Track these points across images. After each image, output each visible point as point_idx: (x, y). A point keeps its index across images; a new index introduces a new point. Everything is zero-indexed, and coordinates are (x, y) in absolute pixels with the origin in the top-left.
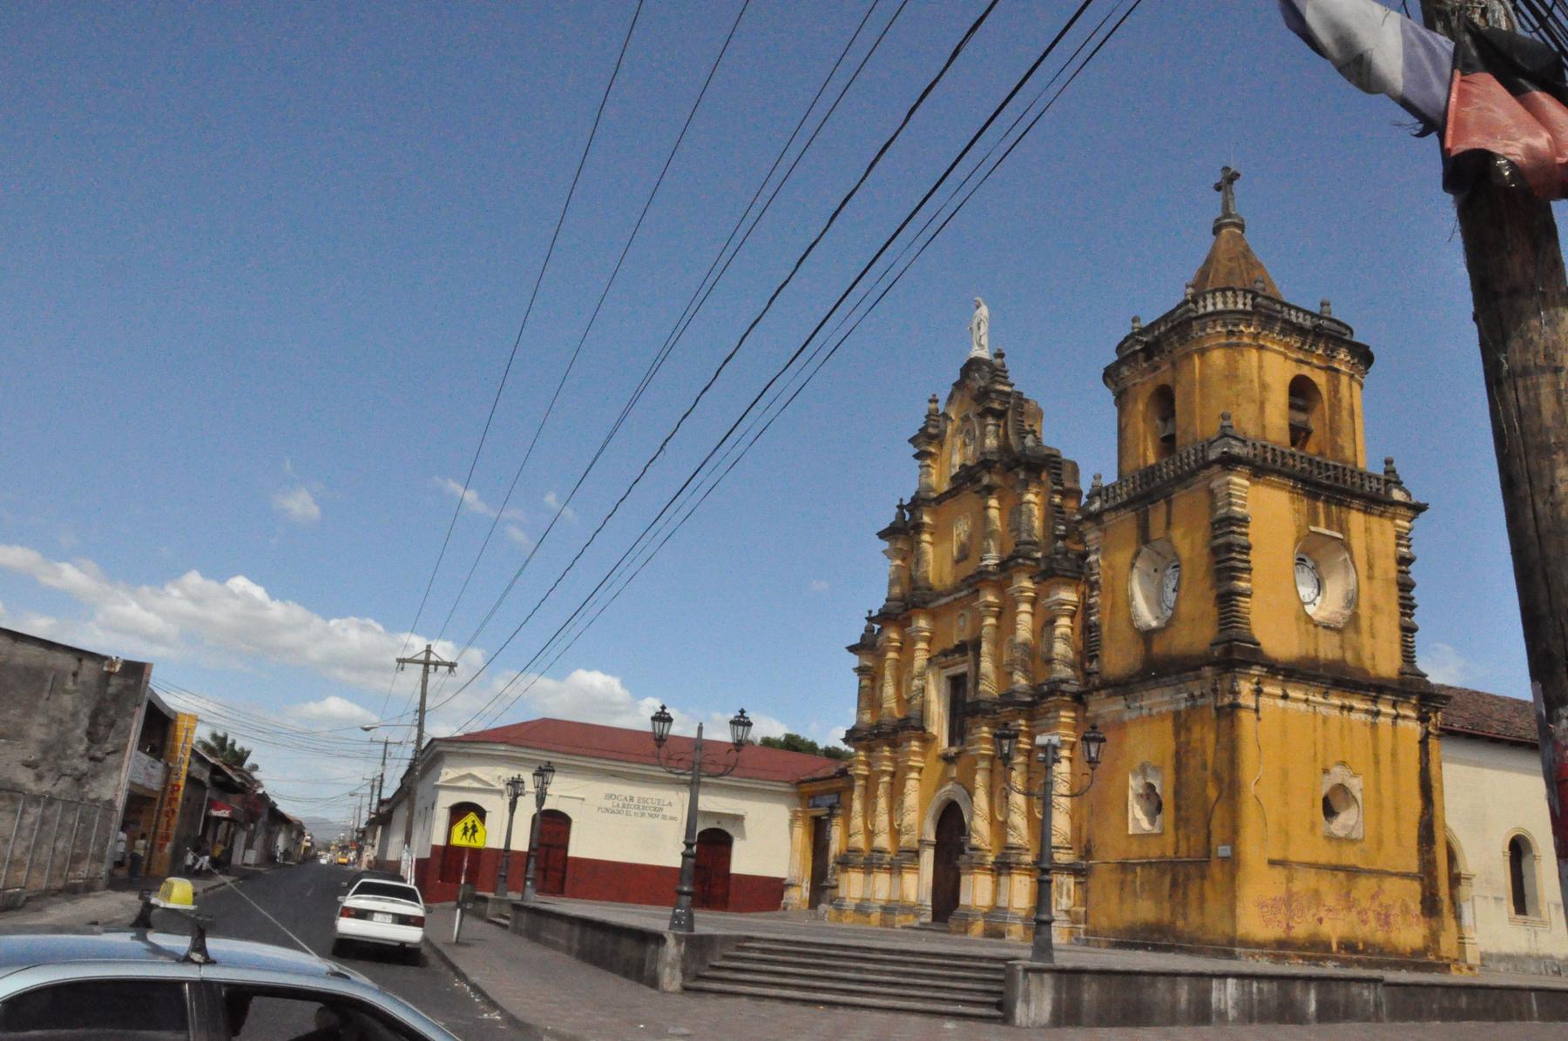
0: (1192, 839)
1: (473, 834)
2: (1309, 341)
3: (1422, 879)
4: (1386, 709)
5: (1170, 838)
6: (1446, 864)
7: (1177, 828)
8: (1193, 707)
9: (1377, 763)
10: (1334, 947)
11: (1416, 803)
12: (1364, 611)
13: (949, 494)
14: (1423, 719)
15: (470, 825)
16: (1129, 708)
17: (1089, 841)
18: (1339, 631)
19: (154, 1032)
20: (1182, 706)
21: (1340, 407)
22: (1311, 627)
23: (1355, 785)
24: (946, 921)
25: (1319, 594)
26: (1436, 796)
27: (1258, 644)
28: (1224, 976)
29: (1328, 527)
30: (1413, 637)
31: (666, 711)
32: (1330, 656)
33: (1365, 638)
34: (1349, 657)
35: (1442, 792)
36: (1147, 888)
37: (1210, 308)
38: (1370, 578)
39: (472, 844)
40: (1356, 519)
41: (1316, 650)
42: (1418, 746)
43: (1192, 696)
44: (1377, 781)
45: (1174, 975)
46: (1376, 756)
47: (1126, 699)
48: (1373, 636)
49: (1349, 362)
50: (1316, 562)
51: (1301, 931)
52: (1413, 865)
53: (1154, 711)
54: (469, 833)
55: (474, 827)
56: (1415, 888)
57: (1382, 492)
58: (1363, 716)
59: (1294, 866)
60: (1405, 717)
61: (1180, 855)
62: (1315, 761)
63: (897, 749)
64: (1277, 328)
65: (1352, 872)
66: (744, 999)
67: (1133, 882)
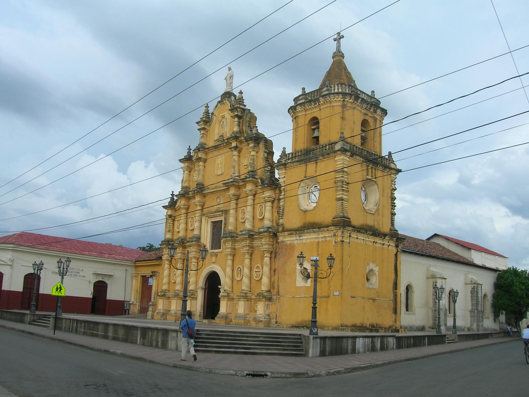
1: (60, 290)
4: (386, 243)
6: (317, 288)
13: (216, 147)
14: (397, 246)
15: (59, 287)
23: (376, 269)
24: (214, 319)
28: (360, 337)
37: (336, 91)
39: (60, 294)
40: (379, 173)
42: (394, 256)
45: (348, 337)
50: (365, 188)
54: (59, 290)
55: (60, 287)
57: (388, 164)
58: (379, 245)
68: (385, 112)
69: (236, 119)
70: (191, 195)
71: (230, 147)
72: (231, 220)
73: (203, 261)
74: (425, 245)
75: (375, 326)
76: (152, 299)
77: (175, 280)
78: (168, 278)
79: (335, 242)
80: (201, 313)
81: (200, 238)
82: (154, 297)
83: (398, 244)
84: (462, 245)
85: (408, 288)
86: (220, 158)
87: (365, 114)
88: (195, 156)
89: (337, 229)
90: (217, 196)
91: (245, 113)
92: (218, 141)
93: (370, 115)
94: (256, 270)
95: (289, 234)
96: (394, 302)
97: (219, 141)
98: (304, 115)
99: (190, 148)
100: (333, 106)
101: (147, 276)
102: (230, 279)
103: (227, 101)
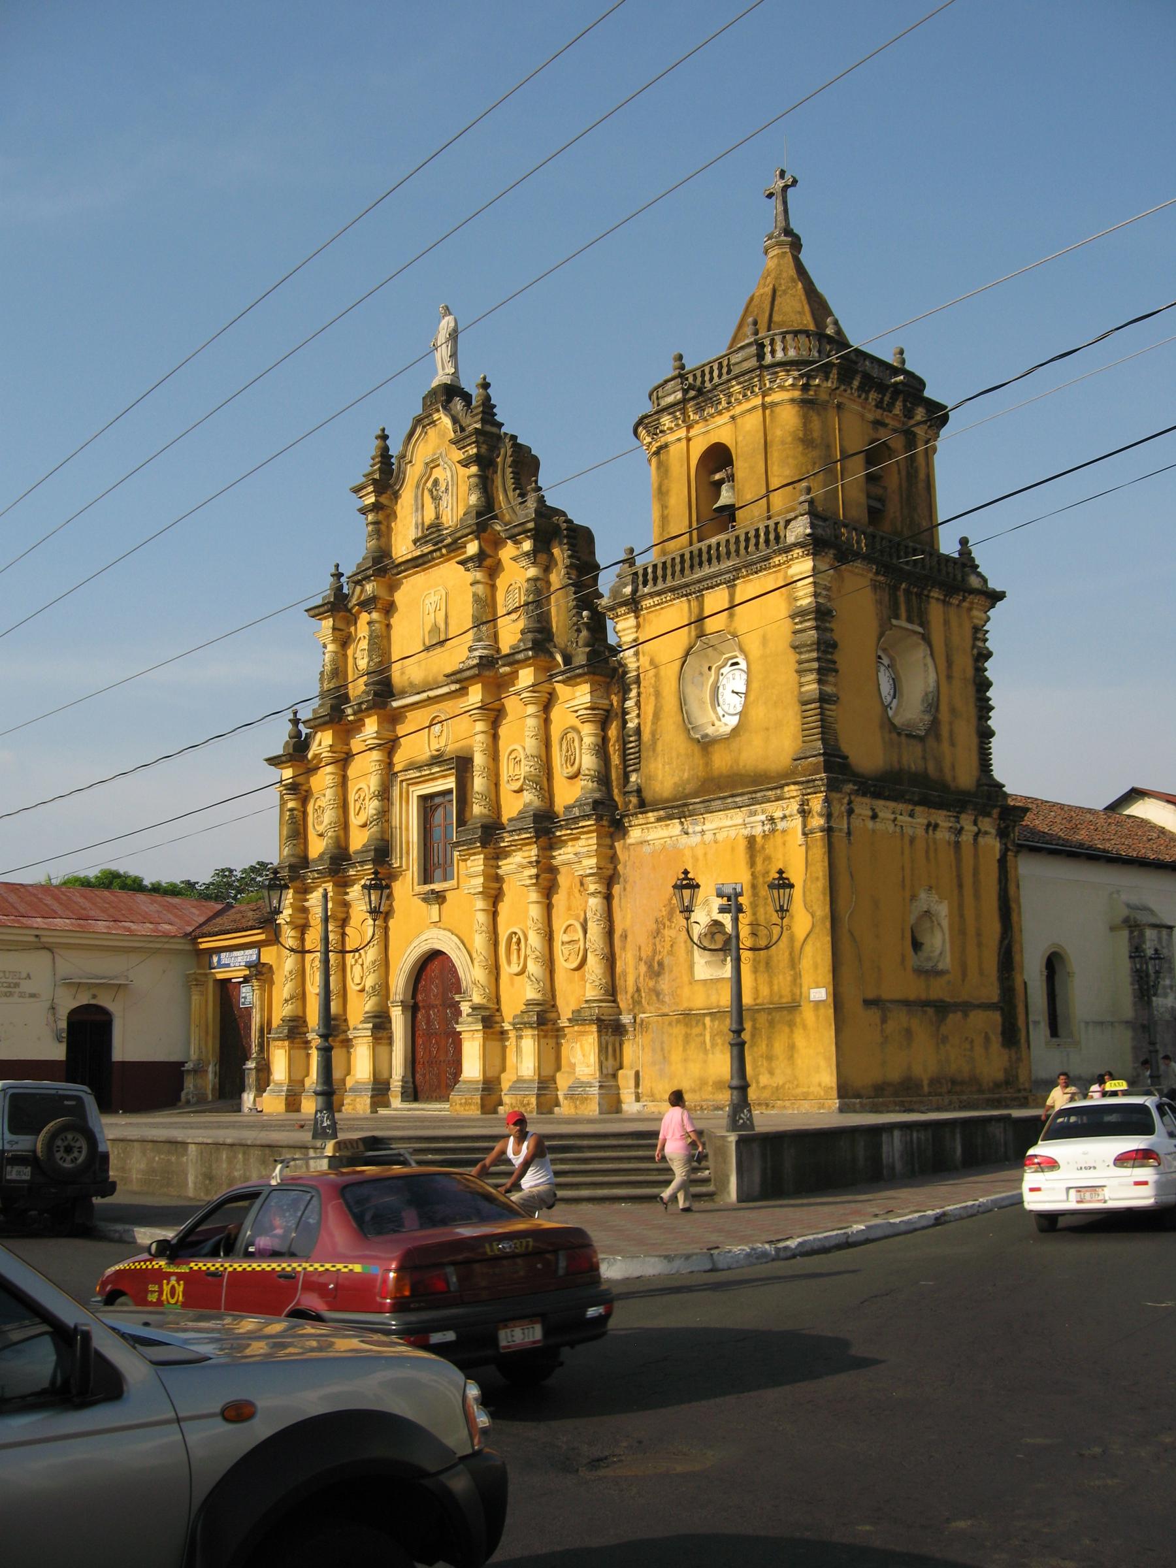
3: (1002, 1009)
8: (773, 831)
9: (960, 886)
11: (993, 927)
12: (944, 715)
16: (687, 833)
18: (921, 739)
20: (758, 831)
21: (916, 477)
22: (894, 735)
25: (894, 697)
26: (1014, 917)
27: (845, 758)
29: (910, 620)
30: (990, 742)
33: (945, 746)
35: (1019, 913)
36: (719, 1041)
38: (949, 677)
43: (772, 820)
44: (961, 906)
46: (959, 877)
47: (682, 823)
48: (953, 744)
50: (892, 659)
52: (992, 993)
53: (720, 837)
56: (997, 1017)
59: (888, 1005)
60: (986, 833)
62: (903, 887)
64: (856, 383)
65: (941, 1009)
67: (702, 1035)
68: (938, 416)
69: (474, 469)
76: (254, 1049)
79: (805, 834)
85: (1053, 964)
87: (878, 424)
94: (566, 938)
95: (659, 820)
100: (774, 405)
101: (233, 980)
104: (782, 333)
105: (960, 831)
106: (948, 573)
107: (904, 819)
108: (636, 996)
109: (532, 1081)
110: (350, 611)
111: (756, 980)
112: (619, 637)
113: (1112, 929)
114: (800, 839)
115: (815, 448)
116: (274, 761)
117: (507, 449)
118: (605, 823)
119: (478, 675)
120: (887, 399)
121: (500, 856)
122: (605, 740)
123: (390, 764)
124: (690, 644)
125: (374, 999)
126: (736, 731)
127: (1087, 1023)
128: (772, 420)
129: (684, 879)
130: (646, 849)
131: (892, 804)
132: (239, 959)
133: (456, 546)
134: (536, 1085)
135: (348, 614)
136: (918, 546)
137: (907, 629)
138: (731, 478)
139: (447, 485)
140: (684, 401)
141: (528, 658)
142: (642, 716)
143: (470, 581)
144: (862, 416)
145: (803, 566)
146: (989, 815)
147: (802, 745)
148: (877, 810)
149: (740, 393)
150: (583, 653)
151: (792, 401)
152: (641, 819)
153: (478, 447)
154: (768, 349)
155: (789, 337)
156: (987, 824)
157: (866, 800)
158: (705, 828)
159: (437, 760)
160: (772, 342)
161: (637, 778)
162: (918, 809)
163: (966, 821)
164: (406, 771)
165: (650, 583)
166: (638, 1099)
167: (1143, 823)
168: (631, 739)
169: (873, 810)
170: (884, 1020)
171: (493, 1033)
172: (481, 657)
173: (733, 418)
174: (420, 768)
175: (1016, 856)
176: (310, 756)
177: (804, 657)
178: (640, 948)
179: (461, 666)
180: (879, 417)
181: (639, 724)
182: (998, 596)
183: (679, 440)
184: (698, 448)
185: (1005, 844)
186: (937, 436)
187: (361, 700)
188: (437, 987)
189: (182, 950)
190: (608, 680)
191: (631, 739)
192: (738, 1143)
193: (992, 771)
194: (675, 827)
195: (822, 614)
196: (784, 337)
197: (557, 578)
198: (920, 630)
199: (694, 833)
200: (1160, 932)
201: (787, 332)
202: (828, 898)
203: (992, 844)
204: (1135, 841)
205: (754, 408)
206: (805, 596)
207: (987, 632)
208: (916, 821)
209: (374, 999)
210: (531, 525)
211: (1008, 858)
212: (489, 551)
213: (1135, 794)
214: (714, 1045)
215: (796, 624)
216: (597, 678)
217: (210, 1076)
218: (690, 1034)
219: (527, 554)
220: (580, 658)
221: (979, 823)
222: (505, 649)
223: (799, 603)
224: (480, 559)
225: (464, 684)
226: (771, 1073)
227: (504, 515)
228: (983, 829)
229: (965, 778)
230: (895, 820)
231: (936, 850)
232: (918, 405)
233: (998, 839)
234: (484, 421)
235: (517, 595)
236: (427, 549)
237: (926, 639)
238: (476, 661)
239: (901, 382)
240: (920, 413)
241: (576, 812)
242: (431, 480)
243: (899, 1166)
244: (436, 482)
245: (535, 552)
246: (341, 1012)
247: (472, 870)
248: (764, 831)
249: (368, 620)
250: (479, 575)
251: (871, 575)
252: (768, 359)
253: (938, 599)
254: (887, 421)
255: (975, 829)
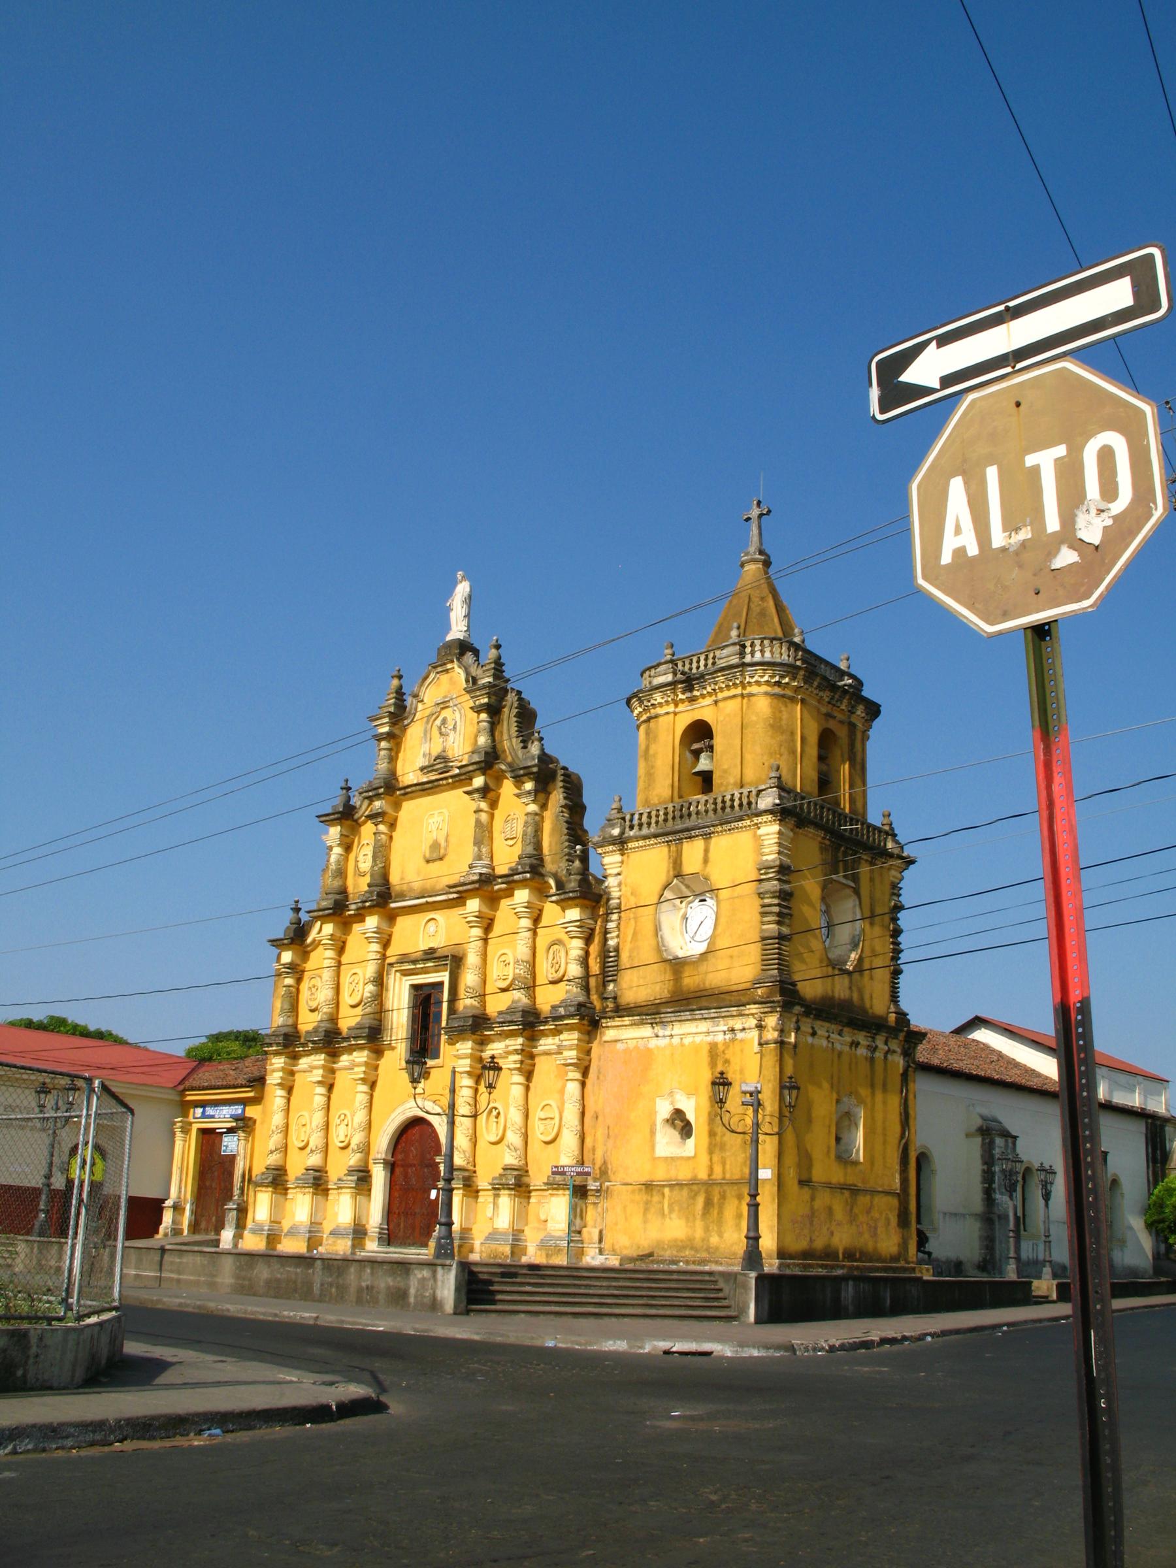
0: (728, 1162)
2: (837, 696)
5: (704, 1158)
7: (711, 1152)
8: (733, 1040)
10: (841, 1256)
11: (897, 1128)
17: (605, 1163)
19: (459, 1336)
20: (720, 1038)
30: (899, 978)
31: (495, 1060)
32: (842, 996)
34: (855, 996)
36: (676, 1208)
41: (833, 992)
43: (733, 1030)
49: (863, 718)
51: (819, 1244)
56: (895, 1202)
60: (894, 1052)
61: (714, 1177)
63: (336, 1059)
66: (523, 1315)
67: (661, 1203)
68: (873, 710)
69: (484, 716)
70: (352, 912)
71: (469, 789)
72: (469, 978)
73: (490, 1093)
74: (954, 1048)
75: (858, 1255)
76: (236, 1192)
77: (303, 1141)
78: (322, 1134)
79: (760, 1044)
80: (382, 1229)
81: (380, 1029)
82: (242, 1189)
83: (909, 1049)
84: (1033, 1041)
86: (436, 815)
87: (829, 716)
88: (364, 807)
89: (766, 1010)
90: (425, 921)
91: (506, 701)
92: (457, 779)
93: (839, 716)
96: (902, 1197)
97: (434, 770)
98: (672, 715)
99: (349, 785)
100: (751, 695)
101: (218, 1131)
102: (468, 1138)
103: (455, 665)
104: (760, 639)
105: (874, 1049)
106: (828, 820)
107: (834, 1036)
108: (603, 1168)
109: (504, 1234)
110: (356, 821)
111: (711, 1160)
112: (605, 869)
113: (968, 1136)
114: (756, 1048)
115: (782, 733)
116: (277, 943)
117: (511, 698)
118: (585, 1022)
119: (477, 889)
120: (837, 696)
121: (485, 1042)
122: (587, 953)
123: (384, 957)
124: (668, 881)
125: (358, 1155)
126: (704, 956)
127: (945, 1214)
128: (748, 707)
129: (720, 1078)
130: (619, 1046)
131: (826, 1024)
132: (224, 1112)
133: (463, 778)
134: (511, 1237)
135: (354, 823)
136: (854, 817)
137: (843, 884)
138: (711, 748)
139: (455, 724)
140: (673, 684)
141: (525, 880)
142: (621, 936)
143: (475, 809)
144: (818, 710)
145: (770, 830)
146: (896, 1037)
147: (761, 972)
148: (816, 1029)
149: (723, 682)
150: (575, 880)
151: (766, 694)
152: (617, 1022)
153: (489, 698)
154: (748, 650)
155: (766, 642)
156: (895, 1045)
157: (808, 1020)
158: (673, 1033)
159: (430, 954)
160: (752, 645)
161: (614, 987)
162: (846, 1029)
163: (880, 1041)
164: (402, 963)
165: (636, 828)
166: (601, 1252)
167: (986, 1047)
168: (611, 954)
169: (813, 1028)
170: (813, 1199)
171: (470, 1191)
172: (481, 874)
173: (716, 702)
174: (414, 962)
175: (914, 1072)
176: (309, 940)
177: (767, 901)
178: (608, 1128)
179: (462, 880)
180: (830, 711)
181: (619, 943)
182: (910, 862)
183: (668, 713)
184: (684, 720)
185: (908, 1062)
186: (871, 727)
187: (364, 899)
188: (416, 1149)
189: (173, 1100)
190: (594, 904)
191: (611, 954)
192: (757, 1279)
193: (899, 1001)
194: (646, 1031)
195: (784, 871)
196: (762, 642)
197: (549, 817)
198: (852, 884)
199: (664, 1036)
200: (1006, 1141)
201: (765, 638)
202: (778, 1098)
203: (899, 1061)
204: (981, 1063)
205: (735, 696)
206: (771, 855)
207: (901, 888)
208: (842, 1040)
209: (358, 1155)
210: (535, 769)
211: (909, 1073)
212: (492, 785)
213: (978, 1022)
214: (671, 1211)
215: (761, 874)
216: (586, 902)
217: (187, 1213)
218: (651, 1201)
219: (529, 793)
220: (572, 884)
221: (889, 1044)
222: (501, 870)
223: (765, 858)
224: (485, 791)
225: (463, 895)
226: (721, 1235)
227: (507, 757)
228: (892, 1048)
229: (879, 1005)
230: (829, 1037)
231: (856, 1063)
232: (859, 704)
233: (902, 1057)
234: (496, 677)
235: (515, 825)
236: (433, 776)
237: (857, 892)
238: (476, 878)
239: (849, 685)
240: (860, 711)
241: (562, 1011)
242: (440, 718)
243: (851, 1308)
244: (444, 721)
245: (536, 791)
246: (324, 1165)
247: (460, 1052)
248: (725, 1039)
249: (375, 831)
250: (484, 805)
251: (819, 839)
252: (748, 659)
253: (867, 861)
254: (835, 715)
255: (886, 1048)
